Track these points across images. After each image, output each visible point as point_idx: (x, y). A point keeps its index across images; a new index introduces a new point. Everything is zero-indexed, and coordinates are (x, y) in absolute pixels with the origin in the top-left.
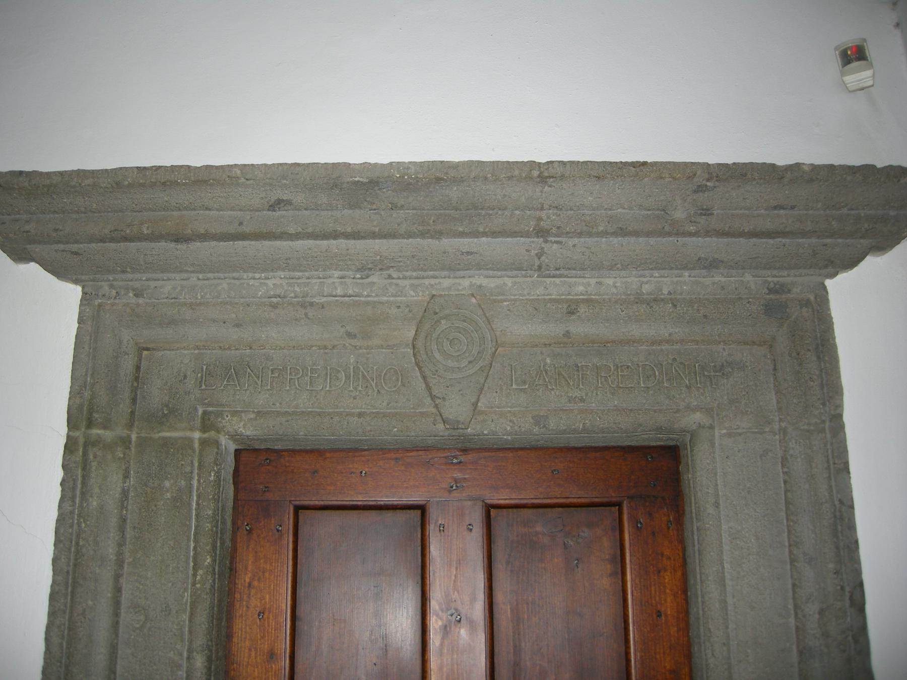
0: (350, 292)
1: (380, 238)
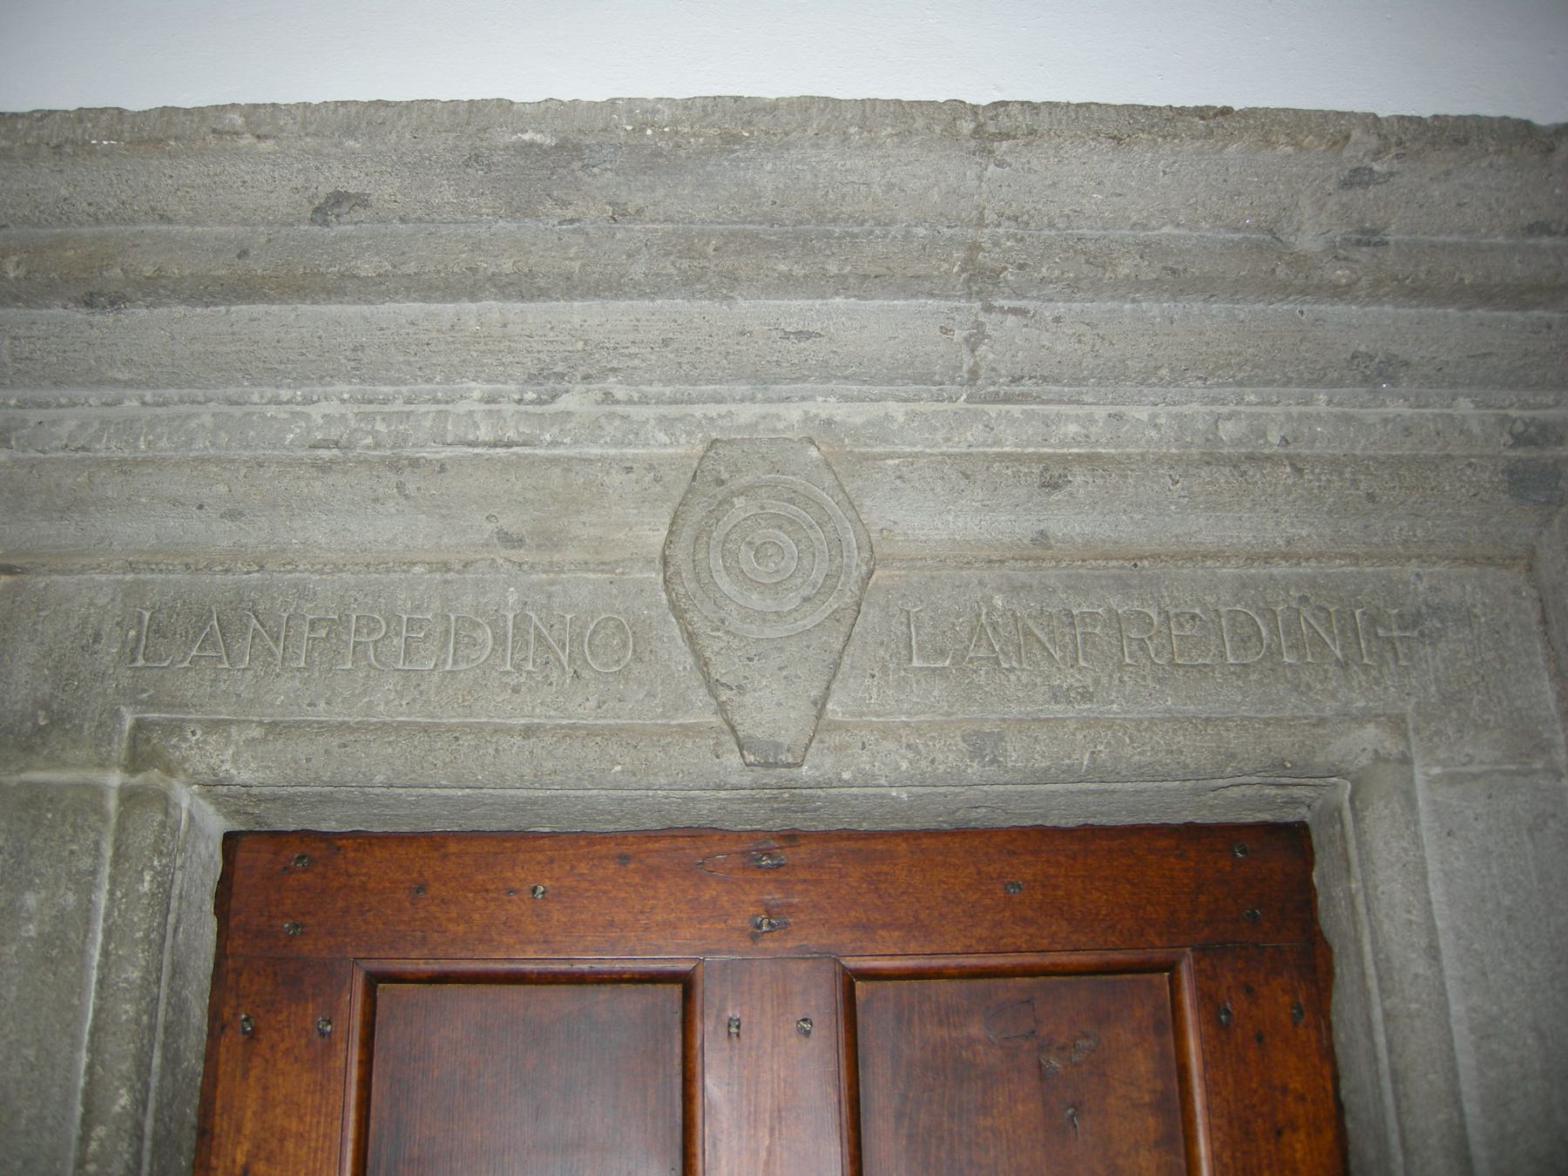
0: (511, 434)
1: (583, 297)
